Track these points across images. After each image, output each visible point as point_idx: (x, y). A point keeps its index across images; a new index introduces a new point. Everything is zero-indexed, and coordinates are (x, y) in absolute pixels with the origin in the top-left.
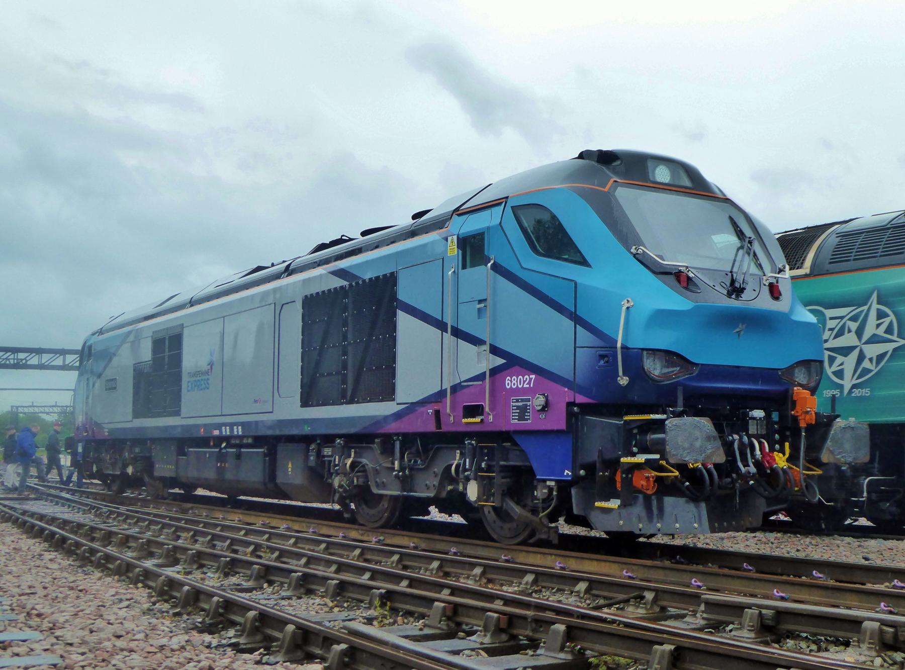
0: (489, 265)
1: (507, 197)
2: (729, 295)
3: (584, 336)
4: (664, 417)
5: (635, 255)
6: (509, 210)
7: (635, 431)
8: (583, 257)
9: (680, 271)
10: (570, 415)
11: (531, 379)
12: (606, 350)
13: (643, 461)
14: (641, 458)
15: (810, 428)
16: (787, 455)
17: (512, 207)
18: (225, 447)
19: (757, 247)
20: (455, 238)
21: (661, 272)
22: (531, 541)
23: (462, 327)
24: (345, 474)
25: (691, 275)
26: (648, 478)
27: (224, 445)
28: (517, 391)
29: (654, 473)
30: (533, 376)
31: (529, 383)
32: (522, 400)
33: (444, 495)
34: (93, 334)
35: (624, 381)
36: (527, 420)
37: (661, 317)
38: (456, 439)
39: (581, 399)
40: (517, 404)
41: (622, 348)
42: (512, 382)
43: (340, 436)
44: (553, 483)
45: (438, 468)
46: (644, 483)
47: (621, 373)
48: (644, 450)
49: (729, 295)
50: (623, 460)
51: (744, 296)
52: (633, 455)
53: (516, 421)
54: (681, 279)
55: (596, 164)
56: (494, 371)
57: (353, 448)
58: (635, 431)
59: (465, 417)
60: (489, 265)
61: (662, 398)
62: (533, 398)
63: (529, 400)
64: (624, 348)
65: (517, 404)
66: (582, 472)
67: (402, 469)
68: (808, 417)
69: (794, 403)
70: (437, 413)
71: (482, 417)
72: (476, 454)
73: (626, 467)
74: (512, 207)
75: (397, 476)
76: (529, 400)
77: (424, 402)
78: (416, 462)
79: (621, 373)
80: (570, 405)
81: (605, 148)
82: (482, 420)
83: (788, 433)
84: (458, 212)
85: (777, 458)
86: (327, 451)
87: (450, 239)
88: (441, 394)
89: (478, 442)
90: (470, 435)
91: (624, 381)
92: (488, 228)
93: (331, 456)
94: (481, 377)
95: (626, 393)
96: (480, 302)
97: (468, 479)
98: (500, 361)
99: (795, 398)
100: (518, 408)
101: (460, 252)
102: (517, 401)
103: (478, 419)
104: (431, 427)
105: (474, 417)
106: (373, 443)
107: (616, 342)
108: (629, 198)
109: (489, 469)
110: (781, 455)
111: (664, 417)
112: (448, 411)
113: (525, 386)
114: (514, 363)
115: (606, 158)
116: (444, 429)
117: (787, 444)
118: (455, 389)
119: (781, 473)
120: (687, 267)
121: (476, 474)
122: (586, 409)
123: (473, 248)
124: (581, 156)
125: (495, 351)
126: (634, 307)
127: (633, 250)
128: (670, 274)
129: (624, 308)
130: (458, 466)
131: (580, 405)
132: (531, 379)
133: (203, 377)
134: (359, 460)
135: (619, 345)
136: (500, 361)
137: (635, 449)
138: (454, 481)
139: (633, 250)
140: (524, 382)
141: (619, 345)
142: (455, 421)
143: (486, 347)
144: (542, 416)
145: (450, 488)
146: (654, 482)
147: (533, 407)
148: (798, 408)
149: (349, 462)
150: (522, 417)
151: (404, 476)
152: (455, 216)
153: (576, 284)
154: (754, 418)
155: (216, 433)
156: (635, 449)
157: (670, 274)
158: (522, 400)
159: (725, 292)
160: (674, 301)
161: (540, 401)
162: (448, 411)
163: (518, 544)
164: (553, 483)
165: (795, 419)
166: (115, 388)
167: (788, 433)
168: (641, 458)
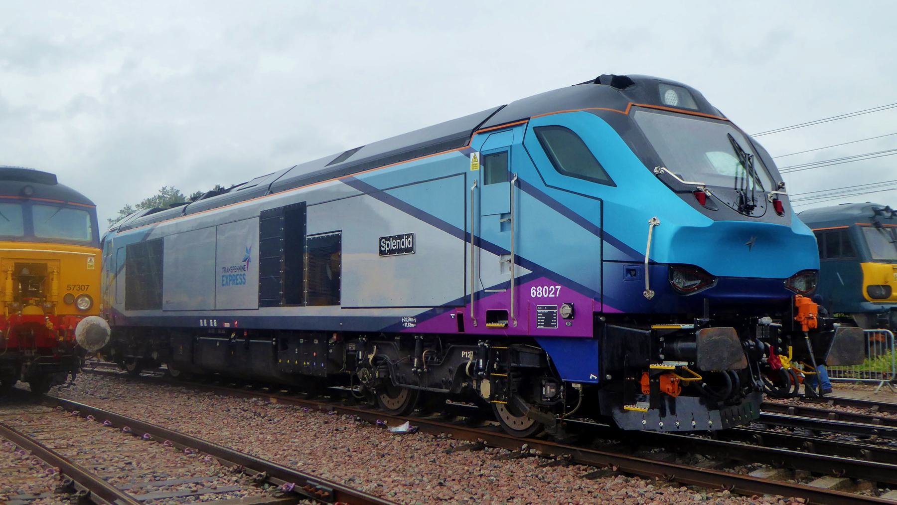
0: (513, 181)
1: (529, 119)
2: (740, 210)
3: (610, 251)
4: (691, 326)
5: (657, 176)
6: (531, 134)
7: (661, 339)
8: (608, 176)
9: (699, 191)
10: (597, 324)
11: (556, 290)
12: (633, 264)
13: (673, 368)
14: (671, 365)
15: (812, 331)
16: (791, 358)
17: (534, 128)
18: (234, 338)
19: (757, 167)
20: (478, 154)
21: (682, 191)
22: (539, 435)
23: (524, 255)
24: (369, 368)
25: (708, 194)
26: (673, 382)
27: (233, 335)
28: (543, 300)
29: (678, 378)
30: (559, 287)
31: (555, 293)
32: (549, 308)
33: (459, 391)
34: (112, 231)
35: (649, 294)
36: (553, 326)
37: (686, 234)
38: (470, 341)
39: (607, 309)
40: (544, 311)
41: (649, 263)
42: (537, 292)
43: (363, 334)
44: (579, 386)
45: (454, 367)
46: (670, 388)
47: (647, 287)
48: (671, 357)
49: (740, 210)
50: (651, 366)
51: (757, 212)
52: (660, 362)
53: (542, 327)
54: (698, 197)
55: (610, 87)
56: (519, 281)
57: (375, 344)
58: (661, 339)
59: (488, 322)
60: (513, 181)
61: (688, 308)
62: (559, 307)
63: (555, 308)
64: (651, 263)
65: (544, 311)
66: (608, 377)
67: (420, 366)
68: (810, 322)
69: (797, 310)
70: (460, 317)
71: (506, 322)
72: (488, 355)
73: (655, 373)
74: (534, 128)
75: (415, 372)
76: (555, 308)
77: (448, 307)
78: (432, 359)
79: (647, 287)
80: (596, 314)
81: (618, 74)
82: (506, 325)
83: (789, 337)
84: (485, 126)
85: (782, 360)
86: (352, 347)
87: (472, 155)
88: (466, 300)
89: (491, 344)
90: (484, 338)
91: (649, 294)
92: (511, 146)
93: (355, 351)
94: (507, 285)
95: (654, 308)
96: (503, 215)
97: (480, 379)
98: (525, 271)
99: (797, 305)
100: (544, 314)
101: (482, 167)
102: (543, 308)
103: (501, 324)
104: (454, 329)
105: (496, 322)
106: (393, 340)
107: (644, 257)
108: (642, 117)
109: (501, 370)
110: (786, 358)
111: (691, 326)
112: (472, 315)
113: (551, 295)
114: (540, 274)
115: (621, 83)
116: (468, 330)
117: (791, 348)
118: (478, 295)
119: (788, 375)
120: (705, 186)
121: (488, 373)
122: (610, 317)
123: (496, 166)
124: (597, 81)
125: (519, 261)
126: (660, 224)
127: (656, 171)
128: (690, 192)
129: (651, 226)
130: (472, 365)
131: (606, 315)
132: (556, 290)
133: (239, 273)
134: (380, 355)
135: (646, 261)
136: (525, 271)
137: (662, 356)
138: (465, 378)
139: (656, 171)
140: (550, 292)
141: (646, 261)
142: (475, 324)
143: (511, 257)
144: (569, 324)
145: (464, 385)
146: (679, 385)
147: (559, 315)
148: (801, 314)
149: (371, 357)
150: (548, 323)
151: (422, 373)
152: (475, 136)
153: (602, 202)
154: (763, 325)
155: (227, 325)
156: (662, 356)
157: (690, 192)
158: (549, 308)
159: (736, 208)
160: (698, 219)
161: (567, 310)
162: (472, 315)
163: (527, 437)
164: (579, 386)
165: (798, 324)
166: (409, 250)
167: (789, 337)
168: (671, 365)
